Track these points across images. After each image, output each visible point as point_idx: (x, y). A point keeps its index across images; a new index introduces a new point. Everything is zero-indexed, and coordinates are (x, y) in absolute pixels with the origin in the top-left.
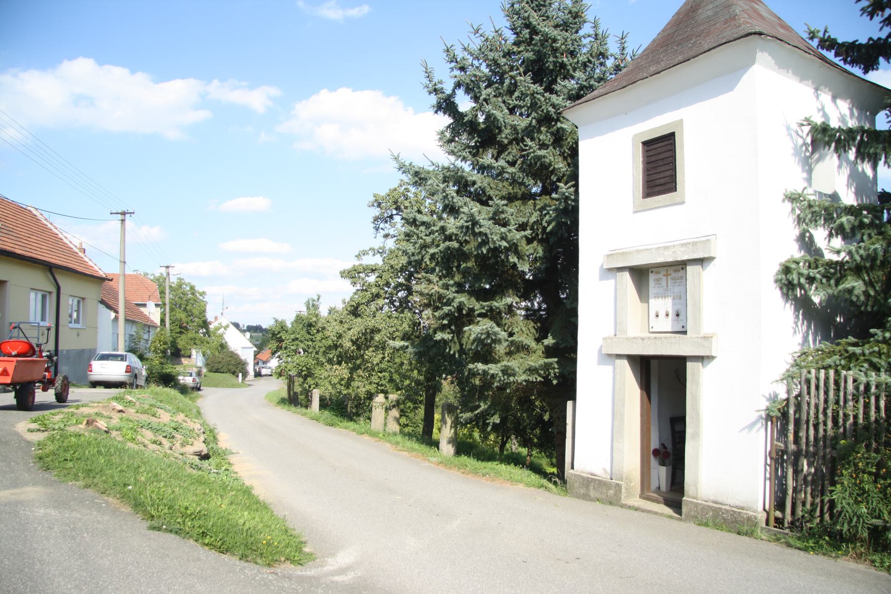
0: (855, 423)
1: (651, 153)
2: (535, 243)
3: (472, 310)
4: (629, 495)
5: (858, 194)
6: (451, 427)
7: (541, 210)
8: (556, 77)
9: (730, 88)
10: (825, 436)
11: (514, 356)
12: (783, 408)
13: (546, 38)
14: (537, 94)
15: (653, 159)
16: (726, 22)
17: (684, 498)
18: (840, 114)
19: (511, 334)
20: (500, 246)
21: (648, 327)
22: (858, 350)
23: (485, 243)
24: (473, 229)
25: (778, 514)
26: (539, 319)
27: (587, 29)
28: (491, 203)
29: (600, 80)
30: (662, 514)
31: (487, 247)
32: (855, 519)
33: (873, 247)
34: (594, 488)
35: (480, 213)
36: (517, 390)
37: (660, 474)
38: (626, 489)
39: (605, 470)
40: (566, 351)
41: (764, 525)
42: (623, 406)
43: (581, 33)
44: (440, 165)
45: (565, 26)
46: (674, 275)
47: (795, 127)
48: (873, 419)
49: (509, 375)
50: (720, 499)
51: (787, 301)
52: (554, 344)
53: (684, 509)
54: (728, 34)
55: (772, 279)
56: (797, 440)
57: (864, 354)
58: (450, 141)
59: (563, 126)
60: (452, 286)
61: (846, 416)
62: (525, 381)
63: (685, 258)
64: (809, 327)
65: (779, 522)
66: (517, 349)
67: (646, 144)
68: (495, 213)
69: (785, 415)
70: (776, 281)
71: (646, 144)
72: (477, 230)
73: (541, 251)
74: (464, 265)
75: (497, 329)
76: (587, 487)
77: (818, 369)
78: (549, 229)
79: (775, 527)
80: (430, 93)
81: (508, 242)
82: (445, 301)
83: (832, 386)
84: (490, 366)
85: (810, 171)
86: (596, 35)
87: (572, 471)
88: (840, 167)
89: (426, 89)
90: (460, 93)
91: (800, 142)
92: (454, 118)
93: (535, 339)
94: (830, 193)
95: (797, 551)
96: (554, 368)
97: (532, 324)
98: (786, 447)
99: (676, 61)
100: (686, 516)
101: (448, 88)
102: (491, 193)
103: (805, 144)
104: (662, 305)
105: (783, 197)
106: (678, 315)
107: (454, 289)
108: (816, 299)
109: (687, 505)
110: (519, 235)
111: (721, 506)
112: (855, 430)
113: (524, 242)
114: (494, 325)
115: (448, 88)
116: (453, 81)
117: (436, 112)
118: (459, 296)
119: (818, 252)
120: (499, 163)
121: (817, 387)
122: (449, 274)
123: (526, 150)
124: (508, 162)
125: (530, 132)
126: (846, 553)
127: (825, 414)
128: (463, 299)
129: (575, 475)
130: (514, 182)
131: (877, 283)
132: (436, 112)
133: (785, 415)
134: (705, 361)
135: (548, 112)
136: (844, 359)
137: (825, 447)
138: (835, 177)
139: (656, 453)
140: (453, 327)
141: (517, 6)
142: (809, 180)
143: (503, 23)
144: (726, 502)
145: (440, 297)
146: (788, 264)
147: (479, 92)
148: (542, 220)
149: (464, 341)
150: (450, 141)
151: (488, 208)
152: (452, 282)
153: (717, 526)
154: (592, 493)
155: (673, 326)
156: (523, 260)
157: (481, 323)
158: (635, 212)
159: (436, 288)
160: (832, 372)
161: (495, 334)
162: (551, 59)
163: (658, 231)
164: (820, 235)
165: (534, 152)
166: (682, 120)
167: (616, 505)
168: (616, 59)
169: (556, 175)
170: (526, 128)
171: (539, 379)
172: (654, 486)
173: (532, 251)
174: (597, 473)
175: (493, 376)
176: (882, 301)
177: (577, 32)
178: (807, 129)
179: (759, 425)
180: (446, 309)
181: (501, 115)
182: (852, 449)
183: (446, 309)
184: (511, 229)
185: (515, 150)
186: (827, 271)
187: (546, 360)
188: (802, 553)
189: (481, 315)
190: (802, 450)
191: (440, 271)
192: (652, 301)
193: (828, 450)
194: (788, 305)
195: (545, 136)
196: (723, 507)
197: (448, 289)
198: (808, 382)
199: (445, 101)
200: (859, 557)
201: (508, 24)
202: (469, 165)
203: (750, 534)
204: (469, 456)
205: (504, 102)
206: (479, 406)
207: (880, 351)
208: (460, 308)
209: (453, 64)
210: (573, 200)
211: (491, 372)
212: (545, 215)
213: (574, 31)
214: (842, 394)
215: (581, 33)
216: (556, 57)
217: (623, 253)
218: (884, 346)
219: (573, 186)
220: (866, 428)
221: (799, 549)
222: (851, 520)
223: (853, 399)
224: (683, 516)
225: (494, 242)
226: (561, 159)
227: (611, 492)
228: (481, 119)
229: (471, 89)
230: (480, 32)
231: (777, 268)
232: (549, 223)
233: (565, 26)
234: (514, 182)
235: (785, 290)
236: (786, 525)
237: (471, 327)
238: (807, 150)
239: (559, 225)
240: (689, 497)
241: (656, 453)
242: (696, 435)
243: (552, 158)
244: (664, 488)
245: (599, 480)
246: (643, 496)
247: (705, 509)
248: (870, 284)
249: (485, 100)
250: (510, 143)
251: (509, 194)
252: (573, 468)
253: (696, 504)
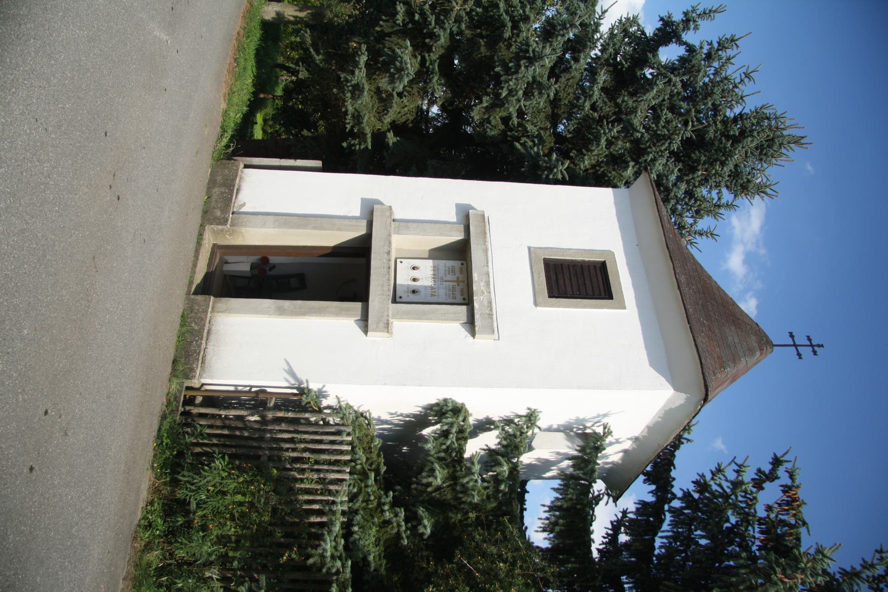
0: (296, 480)
1: (592, 271)
2: (502, 127)
3: (430, 50)
4: (215, 233)
5: (530, 466)
6: (296, 17)
7: (539, 136)
8: (683, 162)
9: (654, 364)
10: (281, 449)
11: (375, 98)
12: (311, 407)
13: (729, 155)
14: (670, 144)
15: (586, 273)
16: (719, 358)
17: (212, 298)
18: (612, 455)
19: (400, 95)
20: (502, 88)
21: (403, 260)
22: (371, 481)
23: (507, 71)
24: (525, 58)
25: (199, 400)
26: (416, 122)
27: (727, 196)
28: (553, 80)
29: (674, 211)
30: (193, 272)
31: (502, 73)
32: (193, 488)
33: (475, 493)
34: (222, 193)
35: (542, 66)
36: (337, 99)
37: (242, 265)
38: (222, 230)
39: (244, 205)
40: (380, 161)
41: (185, 385)
42: (315, 228)
43: (724, 191)
44: (602, 21)
45: (736, 174)
46: (458, 289)
47: (605, 421)
48: (301, 497)
49: (353, 93)
50: (212, 337)
51: (423, 408)
52: (388, 144)
53: (200, 298)
54: (708, 362)
55: (448, 397)
56: (278, 420)
57: (367, 486)
58: (625, 32)
59: (630, 168)
60: (459, 27)
61: (303, 471)
62: (347, 111)
63: (476, 305)
64: (397, 425)
65: (189, 401)
66: (384, 100)
67: (603, 265)
68: (540, 84)
69: (305, 409)
70: (445, 400)
71: (603, 265)
72: (522, 62)
73: (493, 133)
74: (483, 43)
75: (406, 80)
76: (224, 185)
77: (351, 443)
78: (517, 145)
79: (185, 396)
80: (686, 14)
81: (506, 97)
82: (442, 17)
83: (334, 458)
84: (364, 70)
85: (557, 430)
86: (719, 206)
87: (242, 166)
88: (558, 453)
89: (690, 9)
90: (681, 51)
91: (588, 424)
92: (652, 39)
93: (394, 122)
94: (533, 444)
95: (157, 428)
96: (360, 144)
97: (411, 118)
98: (270, 409)
99: (688, 307)
100: (193, 300)
101: (689, 37)
102: (563, 80)
103: (585, 428)
104: (425, 273)
105: (533, 408)
106: (414, 292)
107: (455, 29)
108: (426, 432)
109: (204, 301)
110: (513, 110)
111: (204, 339)
112: (288, 479)
113: (505, 114)
114: (411, 78)
115: (689, 37)
116: (697, 44)
117: (662, 19)
118: (447, 35)
119: (474, 434)
120: (596, 93)
121: (333, 442)
122: (473, 25)
123: (608, 124)
124: (594, 103)
125: (629, 129)
126: (158, 478)
127: (305, 450)
128: (442, 40)
129: (237, 170)
130: (574, 105)
131: (440, 494)
132: (662, 19)
133: (305, 409)
134: (362, 323)
135: (648, 154)
136: (363, 468)
137: (271, 449)
138: (548, 448)
139: (265, 260)
140: (410, 26)
141: (766, 123)
142: (549, 429)
143: (749, 106)
144: (210, 344)
145: (447, 12)
146: (463, 412)
147: (679, 75)
148: (528, 137)
149: (394, 39)
150: (625, 32)
151: (546, 76)
152: (463, 26)
153: (181, 336)
154: (216, 191)
155: (401, 285)
156: (484, 113)
157: (414, 60)
158: (529, 248)
159: (458, 8)
160: (348, 458)
161: (401, 79)
162: (703, 158)
163: (507, 275)
164: (490, 439)
165: (605, 133)
166: (625, 308)
167: (203, 217)
168: (691, 225)
169: (577, 156)
170: (632, 125)
171: (348, 126)
172: (230, 258)
173: (493, 122)
174: (240, 196)
175: (353, 73)
176: (421, 498)
177: (727, 187)
178: (600, 430)
179: (293, 382)
180: (432, 19)
181: (651, 97)
182: (268, 478)
183: (432, 19)
184: (521, 103)
185: (608, 109)
186: (453, 449)
187: (369, 135)
188: (155, 434)
189: (423, 62)
190: (267, 425)
191: (477, 13)
192: (430, 263)
193: (267, 452)
194: (420, 409)
195: (621, 146)
196: (204, 342)
197: (455, 22)
198: (339, 433)
199: (673, 31)
200: (156, 490)
201: (747, 111)
202: (596, 55)
203: (174, 373)
204: (260, 40)
205: (664, 100)
206: (318, 53)
207: (370, 500)
208: (433, 36)
209: (716, 45)
210: (547, 176)
211: (357, 72)
212: (533, 141)
213: (729, 184)
214: (325, 467)
215: (724, 190)
216: (704, 163)
217: (485, 233)
218: (375, 504)
219: (563, 177)
220: (291, 489)
221: (160, 430)
222: (193, 484)
223: (320, 478)
224: (193, 297)
225: (507, 82)
226: (594, 162)
227: (218, 213)
228: (648, 72)
229: (686, 64)
230: (746, 80)
231: (459, 400)
232: (523, 145)
233: (736, 174)
234: (574, 105)
235: (436, 408)
236: (187, 408)
237: (410, 48)
238: (580, 429)
239: (521, 158)
240: (214, 303)
241: (265, 260)
242: (281, 312)
243: (596, 152)
244: (227, 268)
245: (231, 199)
246: (215, 247)
247: (201, 321)
248: (438, 488)
249: (670, 80)
250: (617, 105)
251: (560, 100)
252: (246, 167)
253: (207, 312)
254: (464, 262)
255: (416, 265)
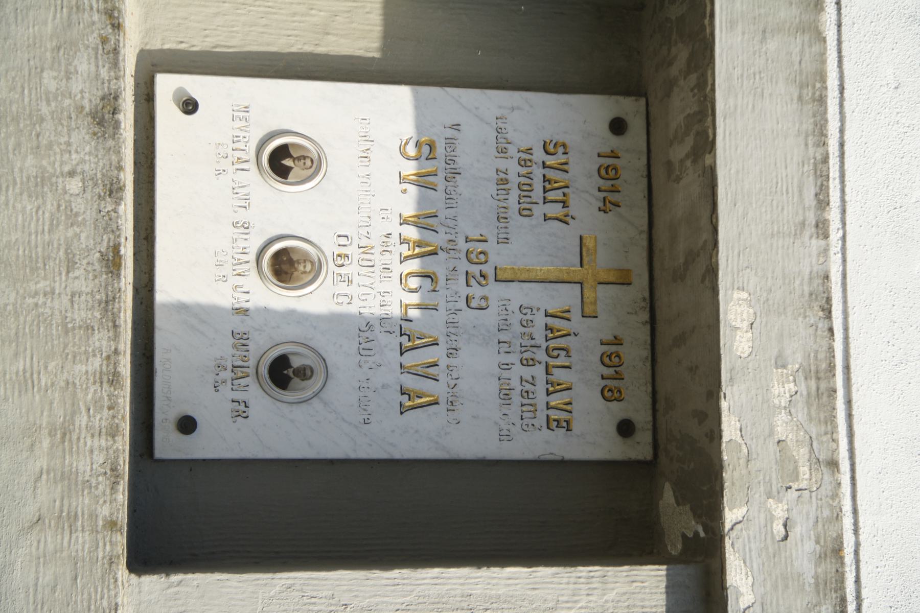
46: (586, 340)
106: (282, 373)
155: (194, 315)
192: (392, 110)
254: (628, 107)
255: (260, 399)
